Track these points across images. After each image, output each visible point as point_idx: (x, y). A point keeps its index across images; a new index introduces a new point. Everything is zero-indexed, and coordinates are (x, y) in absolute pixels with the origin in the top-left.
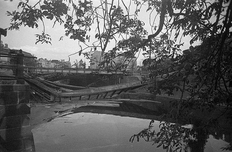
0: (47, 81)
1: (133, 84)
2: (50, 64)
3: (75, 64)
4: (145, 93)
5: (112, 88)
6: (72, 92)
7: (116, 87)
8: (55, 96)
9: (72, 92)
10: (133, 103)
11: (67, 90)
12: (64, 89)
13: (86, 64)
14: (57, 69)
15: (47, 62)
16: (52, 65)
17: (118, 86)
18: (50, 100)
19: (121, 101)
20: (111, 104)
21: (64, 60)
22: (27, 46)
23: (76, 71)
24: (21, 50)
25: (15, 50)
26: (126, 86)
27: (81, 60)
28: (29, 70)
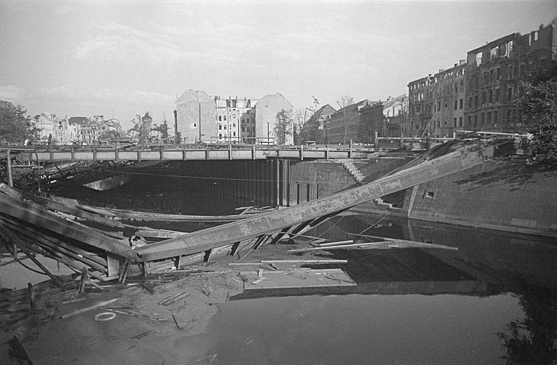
0: (89, 211)
1: (360, 194)
2: (67, 128)
3: (137, 126)
4: (372, 211)
5: (304, 211)
6: (180, 238)
7: (313, 209)
8: (121, 259)
9: (180, 238)
10: (348, 249)
11: (161, 233)
12: (151, 232)
13: (168, 126)
14: (101, 151)
15: (59, 125)
16: (71, 134)
17: (320, 205)
18: (107, 274)
19: (330, 250)
20: (317, 272)
21: (102, 117)
22: (71, 144)
23: (158, 153)
24: (411, 85)
25: (441, 74)
26: (342, 203)
27: (147, 114)
28: (13, 156)
